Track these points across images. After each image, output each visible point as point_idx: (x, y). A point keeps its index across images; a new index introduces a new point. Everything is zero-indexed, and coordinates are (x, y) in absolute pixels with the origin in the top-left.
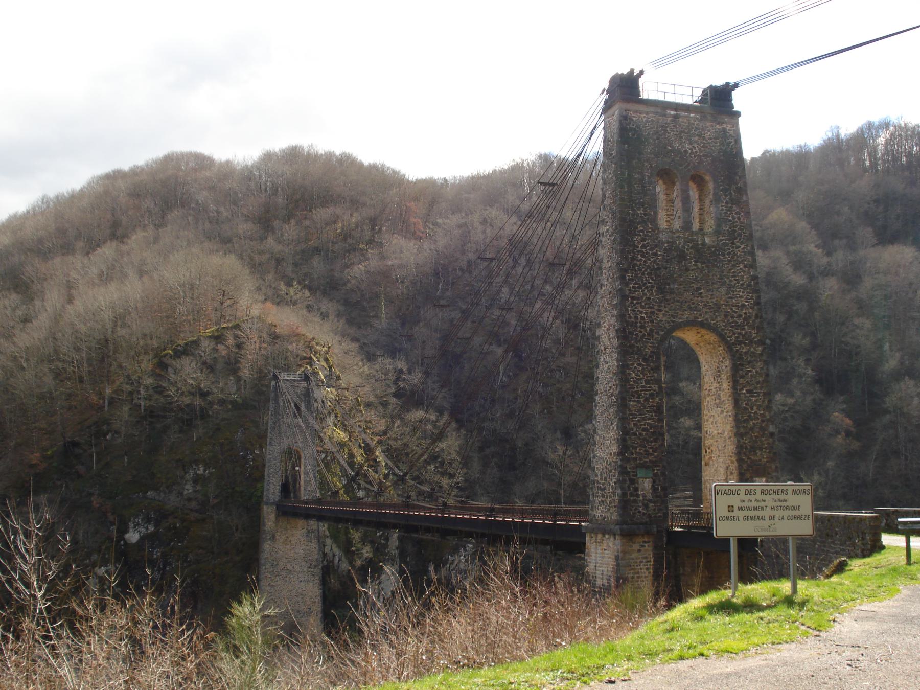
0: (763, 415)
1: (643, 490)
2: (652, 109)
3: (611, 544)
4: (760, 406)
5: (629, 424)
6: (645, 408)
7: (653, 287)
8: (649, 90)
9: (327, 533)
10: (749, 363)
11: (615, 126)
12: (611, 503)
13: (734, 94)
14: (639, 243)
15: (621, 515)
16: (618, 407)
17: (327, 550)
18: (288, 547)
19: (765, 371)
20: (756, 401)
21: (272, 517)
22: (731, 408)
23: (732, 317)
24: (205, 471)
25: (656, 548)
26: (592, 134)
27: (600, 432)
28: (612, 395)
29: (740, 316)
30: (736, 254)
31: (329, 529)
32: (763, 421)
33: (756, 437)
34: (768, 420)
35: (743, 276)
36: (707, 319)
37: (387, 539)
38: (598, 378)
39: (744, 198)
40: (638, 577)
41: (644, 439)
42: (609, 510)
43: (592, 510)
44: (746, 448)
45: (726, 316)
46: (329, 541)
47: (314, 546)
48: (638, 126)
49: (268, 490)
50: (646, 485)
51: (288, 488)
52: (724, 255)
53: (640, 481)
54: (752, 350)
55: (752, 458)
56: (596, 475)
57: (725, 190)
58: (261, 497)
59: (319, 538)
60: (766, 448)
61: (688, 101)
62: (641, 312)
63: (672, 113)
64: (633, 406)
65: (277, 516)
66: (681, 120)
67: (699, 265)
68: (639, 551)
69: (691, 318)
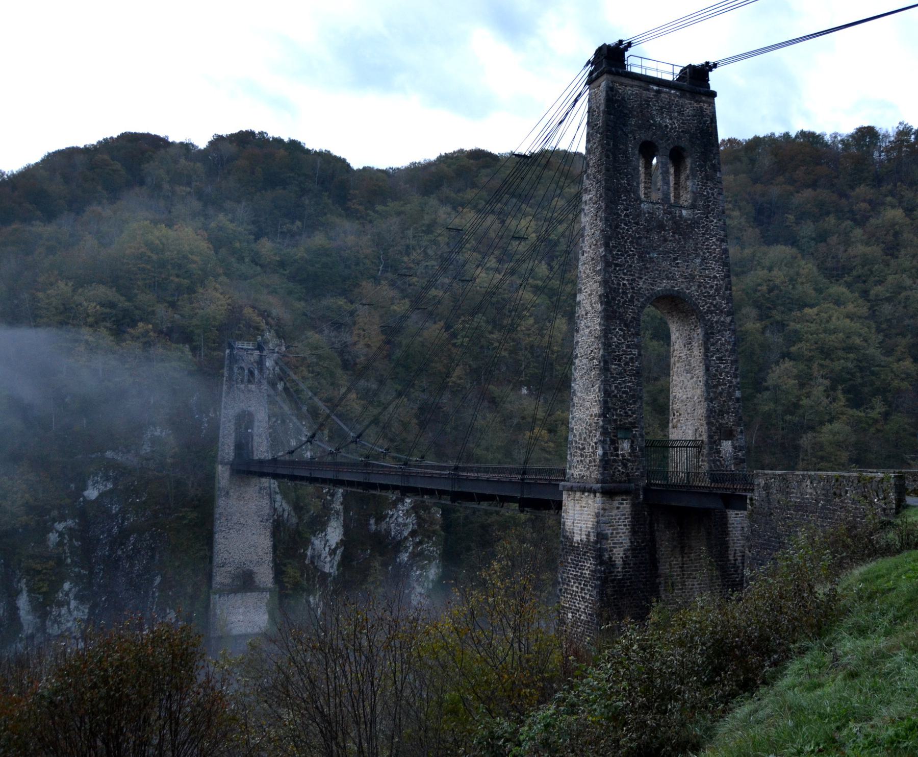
1: (622, 450)
2: (636, 83)
3: (590, 502)
4: (728, 373)
5: (610, 386)
6: (625, 371)
8: (635, 63)
9: (277, 490)
10: (719, 331)
11: (602, 96)
12: (590, 462)
13: (711, 75)
14: (622, 212)
15: (602, 474)
16: (601, 370)
17: (277, 505)
18: (241, 503)
20: (725, 368)
21: (227, 474)
22: (702, 373)
23: (705, 288)
24: (161, 432)
25: (634, 505)
26: (576, 101)
27: (579, 394)
28: (594, 358)
31: (279, 487)
33: (724, 401)
34: (735, 386)
35: (715, 249)
37: (332, 495)
38: (578, 342)
39: (718, 175)
40: (617, 533)
41: (625, 401)
42: (588, 469)
43: (570, 469)
45: (699, 286)
46: (278, 497)
47: (265, 502)
48: (623, 99)
49: (223, 450)
51: (242, 446)
52: (698, 228)
53: (620, 441)
54: (722, 319)
56: (575, 436)
57: (701, 166)
58: (215, 457)
59: (270, 495)
61: (669, 78)
62: (624, 279)
63: (655, 88)
64: (615, 369)
65: (232, 475)
66: (662, 95)
67: (677, 236)
68: (618, 508)
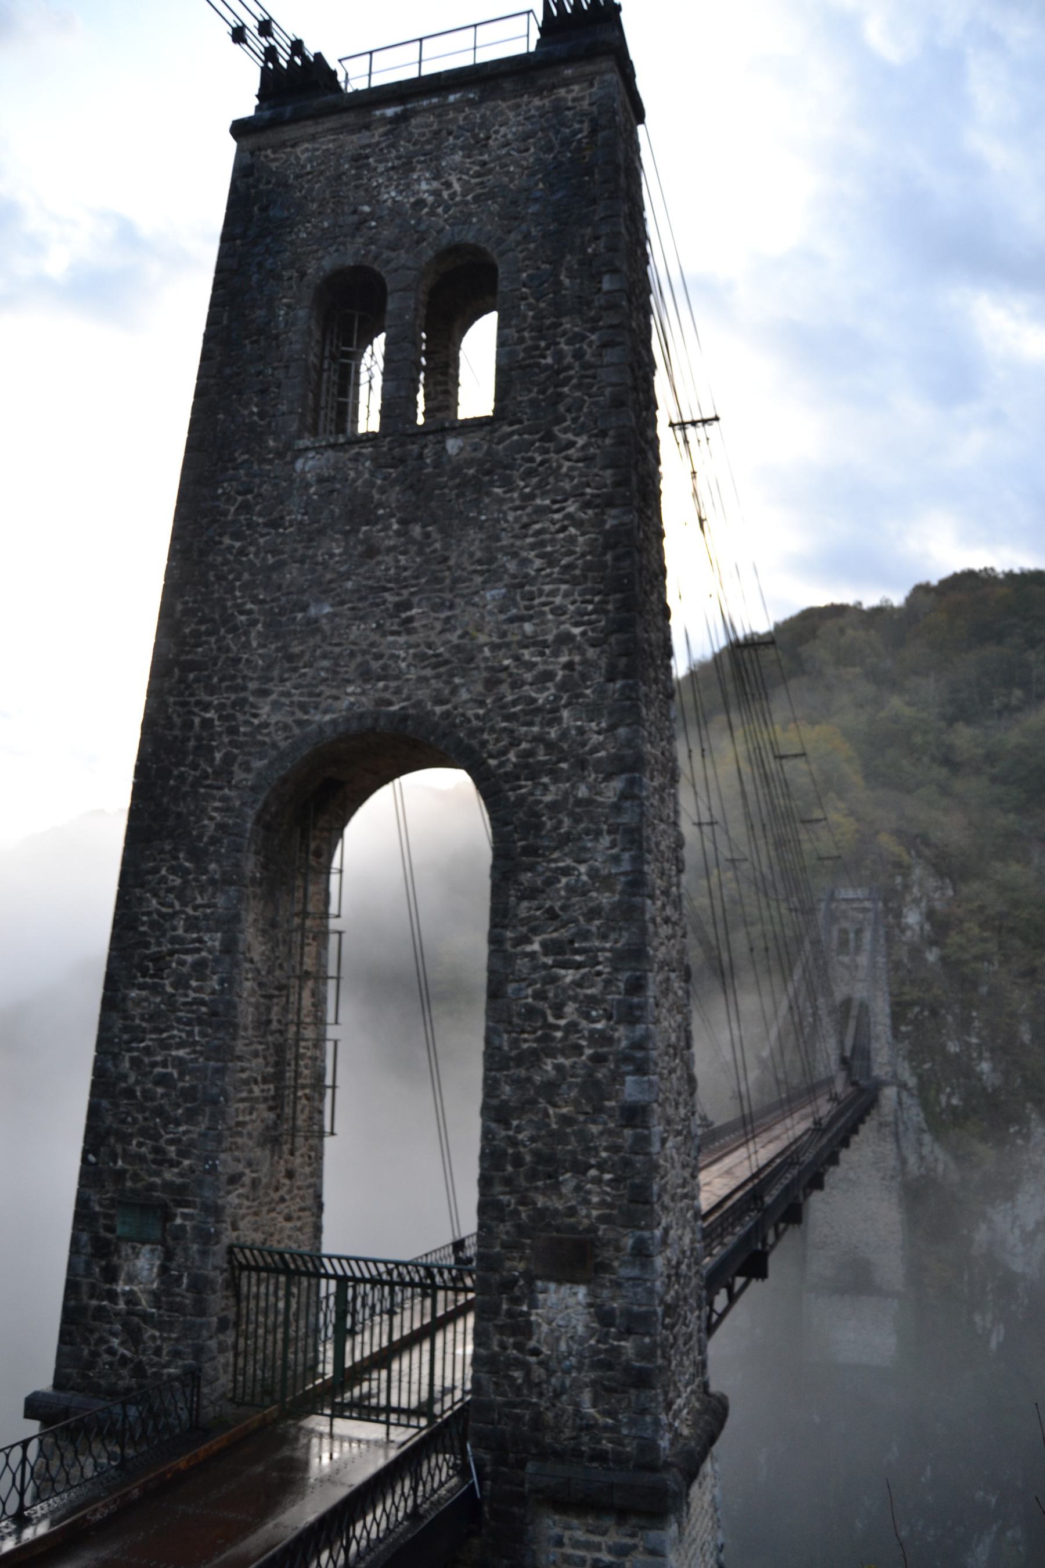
0: (603, 1039)
1: (131, 1279)
4: (593, 1001)
7: (254, 623)
9: (924, 1126)
19: (626, 866)
20: (578, 984)
29: (547, 676)
30: (556, 472)
36: (419, 704)
45: (491, 684)
53: (126, 1249)
54: (582, 792)
55: (541, 1201)
60: (601, 1167)
62: (206, 707)
64: (138, 1002)
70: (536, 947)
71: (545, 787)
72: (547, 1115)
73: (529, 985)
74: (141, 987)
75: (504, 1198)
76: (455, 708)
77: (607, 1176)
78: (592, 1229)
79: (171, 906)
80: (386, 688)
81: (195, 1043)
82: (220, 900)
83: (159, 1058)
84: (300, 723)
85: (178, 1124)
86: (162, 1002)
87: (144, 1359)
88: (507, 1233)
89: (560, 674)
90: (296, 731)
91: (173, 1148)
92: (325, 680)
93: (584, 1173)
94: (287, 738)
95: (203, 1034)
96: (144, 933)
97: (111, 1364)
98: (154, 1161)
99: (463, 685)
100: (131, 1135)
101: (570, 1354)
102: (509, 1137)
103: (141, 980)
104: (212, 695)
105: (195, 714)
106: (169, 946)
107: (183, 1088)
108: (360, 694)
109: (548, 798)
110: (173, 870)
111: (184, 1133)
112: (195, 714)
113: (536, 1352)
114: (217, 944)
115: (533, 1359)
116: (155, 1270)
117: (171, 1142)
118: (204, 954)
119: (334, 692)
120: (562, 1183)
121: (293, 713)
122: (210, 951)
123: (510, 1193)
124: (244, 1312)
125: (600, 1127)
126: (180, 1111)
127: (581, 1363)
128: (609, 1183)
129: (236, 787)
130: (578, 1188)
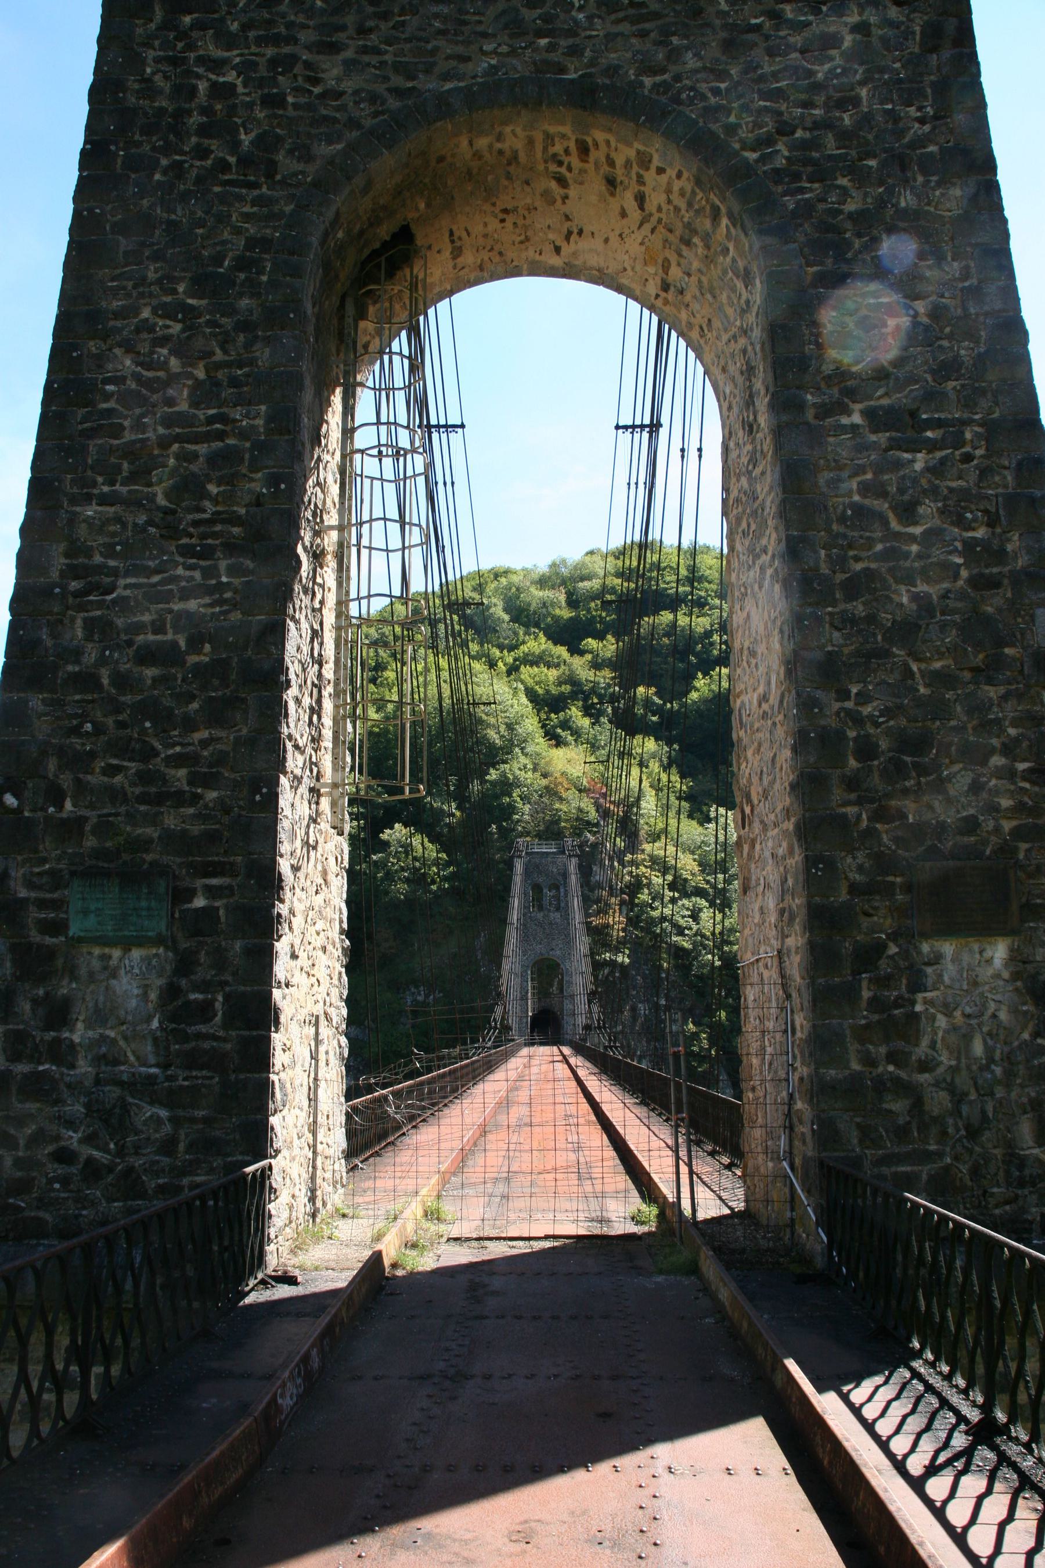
24: (427, 996)
32: (983, 584)
33: (942, 679)
36: (613, 71)
44: (866, 751)
50: (126, 986)
53: (91, 957)
62: (217, 65)
64: (99, 526)
69: (520, 67)
70: (857, 419)
71: (845, 192)
72: (909, 673)
73: (856, 474)
74: (104, 500)
75: (851, 810)
76: (677, 78)
77: (1022, 766)
78: (1006, 850)
79: (164, 366)
80: (551, 48)
81: (221, 587)
82: (263, 355)
83: (146, 618)
84: (399, 93)
85: (189, 725)
86: (150, 523)
87: (138, 1162)
88: (860, 868)
89: (848, 41)
90: (393, 103)
91: (182, 773)
92: (442, 32)
93: (984, 763)
94: (376, 114)
95: (231, 571)
96: (110, 412)
97: (65, 1181)
98: (142, 799)
99: (687, 48)
100: (92, 755)
101: (991, 1060)
102: (848, 712)
103: (106, 489)
104: (229, 49)
105: (199, 77)
106: (161, 430)
107: (197, 665)
108: (508, 55)
109: (851, 207)
110: (167, 312)
111: (204, 743)
112: (199, 77)
113: (925, 1066)
114: (260, 422)
115: (924, 1078)
116: (153, 996)
117: (178, 761)
118: (231, 441)
119: (460, 49)
120: (949, 779)
121: (386, 79)
122: (243, 435)
123: (859, 802)
124: (236, 1238)
125: (1002, 690)
126: (195, 705)
127: (1010, 1074)
128: (1026, 775)
129: (283, 183)
130: (976, 787)
